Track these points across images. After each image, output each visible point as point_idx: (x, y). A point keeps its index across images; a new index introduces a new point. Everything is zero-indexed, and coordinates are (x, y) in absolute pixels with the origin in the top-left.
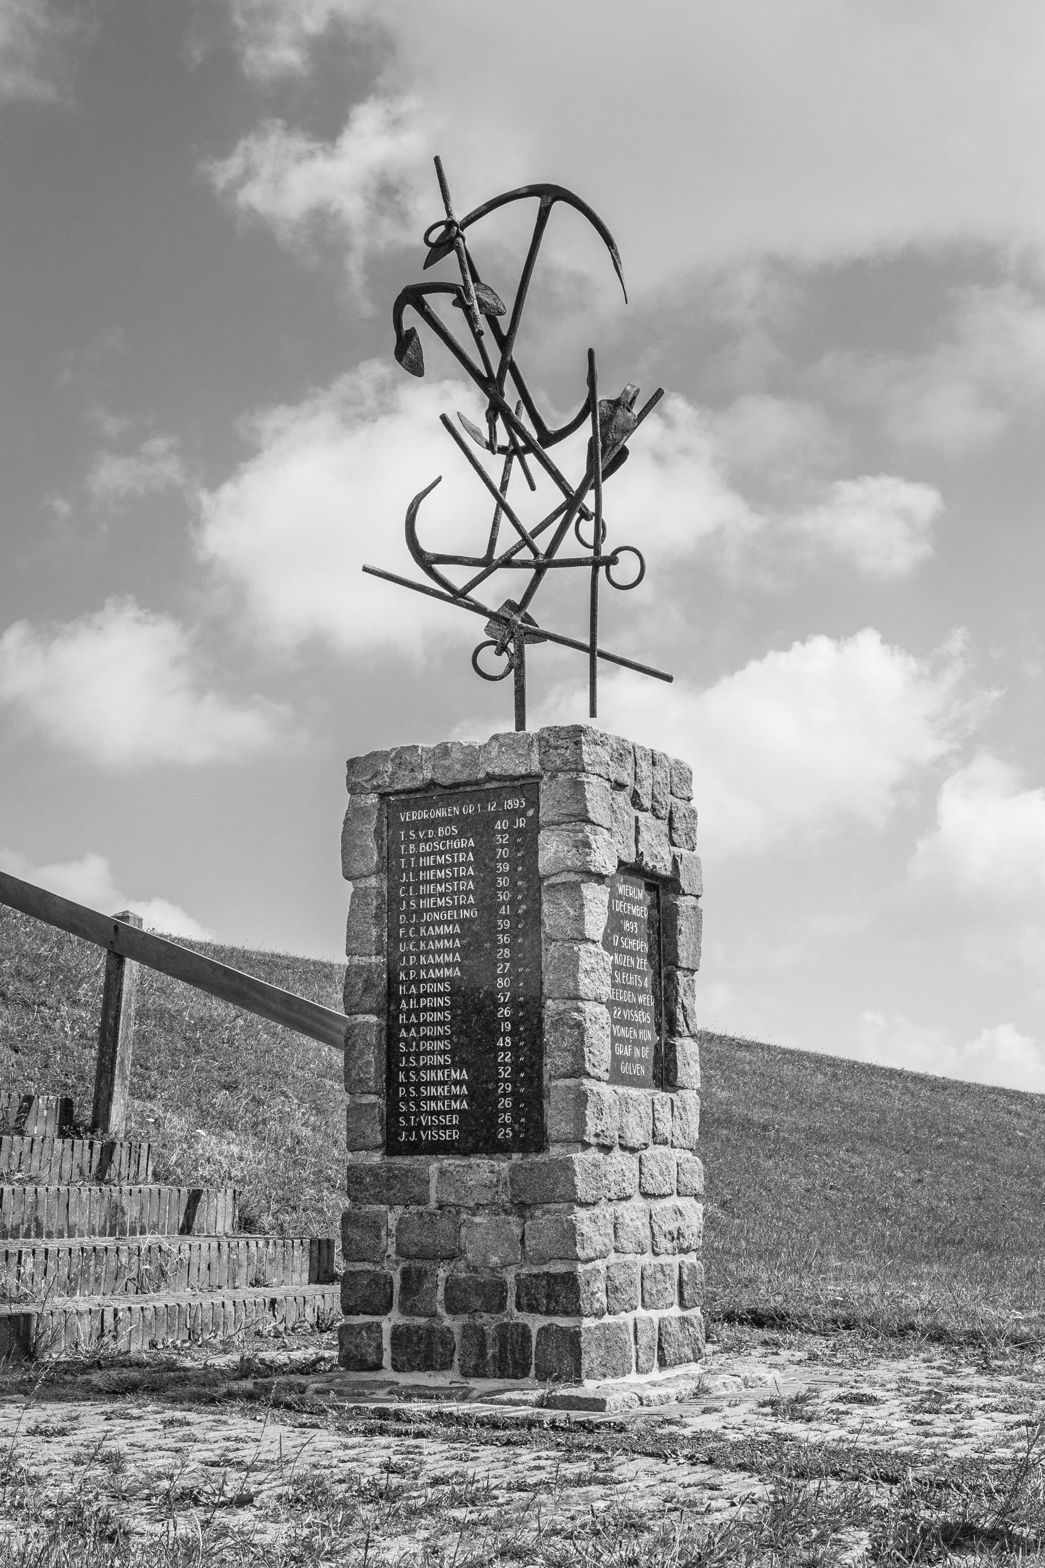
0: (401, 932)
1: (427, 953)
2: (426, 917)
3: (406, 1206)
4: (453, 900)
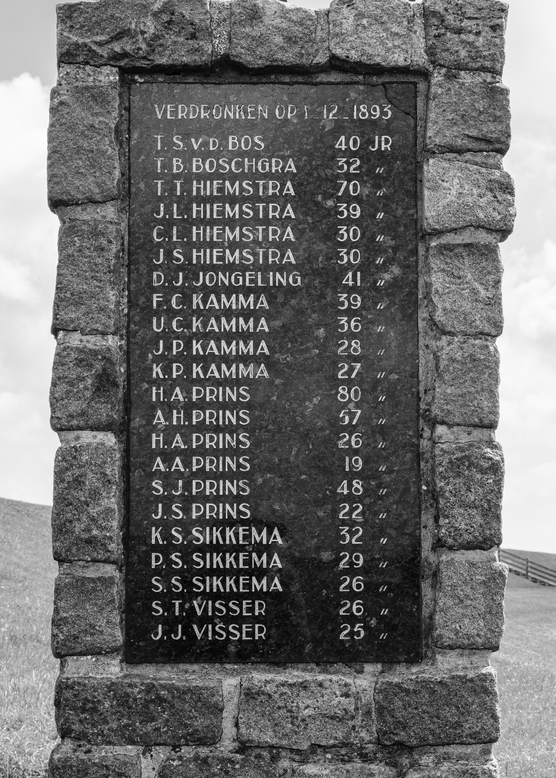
1: (205, 336)
3: (175, 747)
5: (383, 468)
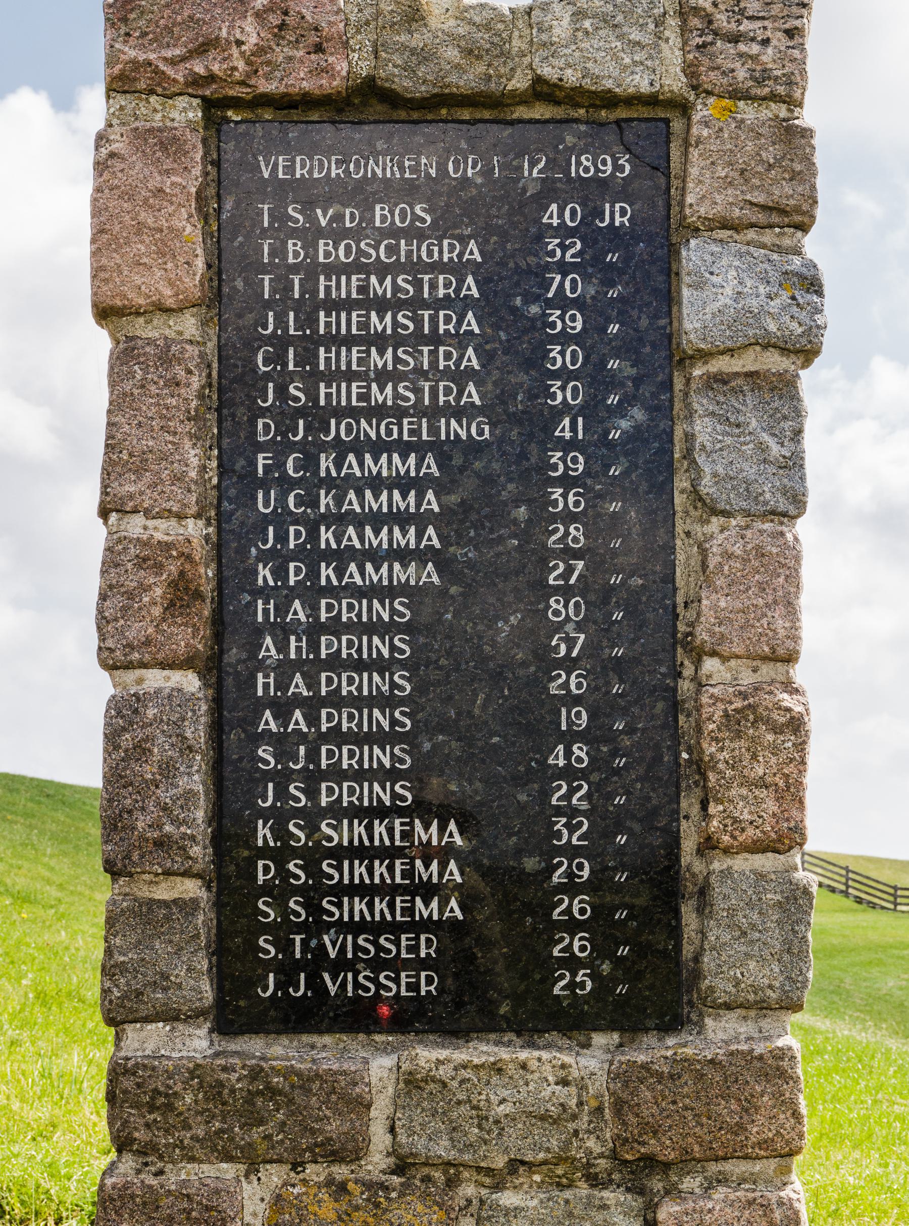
0: (261, 462)
1: (340, 520)
2: (337, 429)
4: (418, 391)
5: (619, 726)
